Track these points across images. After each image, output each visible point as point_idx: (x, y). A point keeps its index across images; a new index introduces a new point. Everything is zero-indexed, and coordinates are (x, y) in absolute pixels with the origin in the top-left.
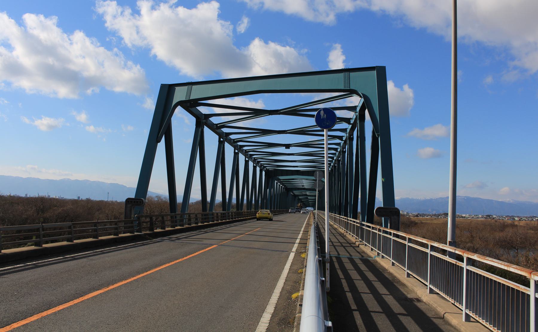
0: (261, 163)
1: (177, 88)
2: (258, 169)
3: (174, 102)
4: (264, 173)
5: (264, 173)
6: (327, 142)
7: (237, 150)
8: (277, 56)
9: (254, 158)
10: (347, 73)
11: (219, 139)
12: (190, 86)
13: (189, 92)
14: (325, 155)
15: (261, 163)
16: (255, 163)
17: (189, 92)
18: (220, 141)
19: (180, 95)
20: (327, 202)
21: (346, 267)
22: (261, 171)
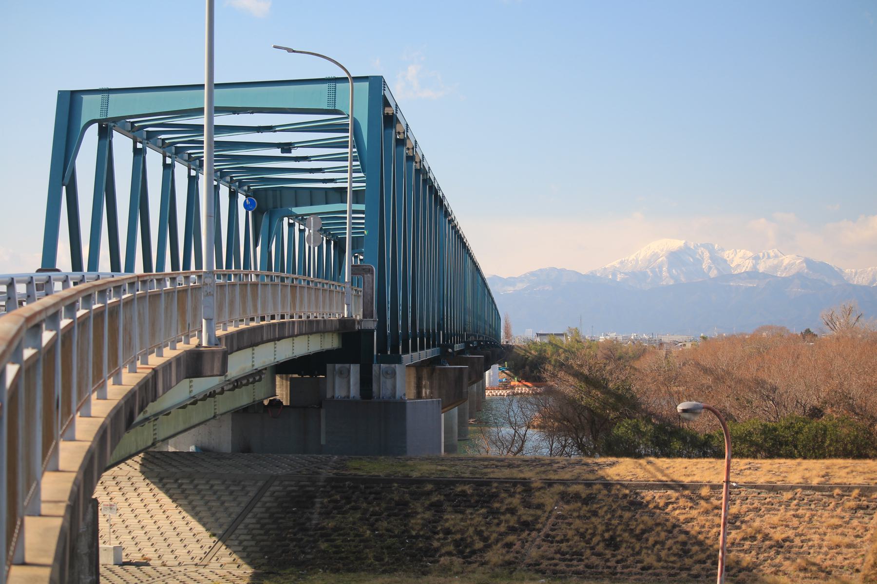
0: (189, 152)
1: (85, 98)
2: (224, 192)
3: (83, 122)
4: (241, 198)
5: (241, 198)
6: (350, 215)
7: (140, 142)
8: (474, 446)
9: (164, 140)
10: (332, 84)
11: (164, 160)
12: (106, 95)
13: (105, 105)
14: (347, 221)
15: (189, 152)
16: (192, 167)
17: (105, 105)
18: (165, 166)
19: (90, 109)
20: (349, 245)
21: (100, 528)
22: (233, 196)
